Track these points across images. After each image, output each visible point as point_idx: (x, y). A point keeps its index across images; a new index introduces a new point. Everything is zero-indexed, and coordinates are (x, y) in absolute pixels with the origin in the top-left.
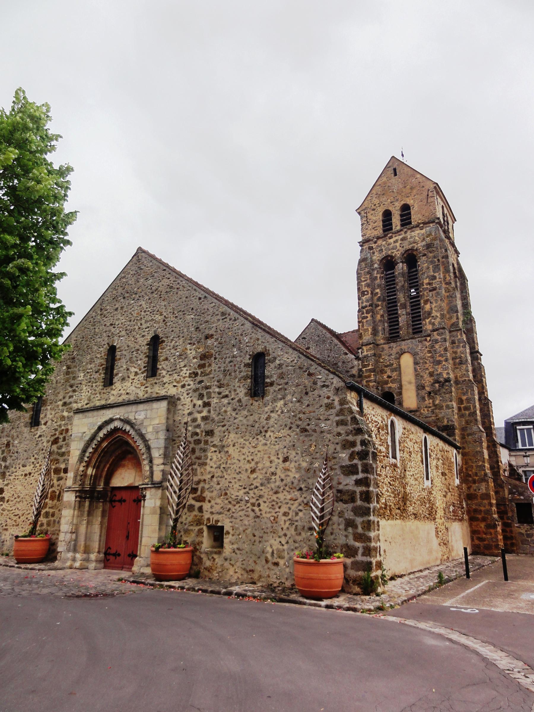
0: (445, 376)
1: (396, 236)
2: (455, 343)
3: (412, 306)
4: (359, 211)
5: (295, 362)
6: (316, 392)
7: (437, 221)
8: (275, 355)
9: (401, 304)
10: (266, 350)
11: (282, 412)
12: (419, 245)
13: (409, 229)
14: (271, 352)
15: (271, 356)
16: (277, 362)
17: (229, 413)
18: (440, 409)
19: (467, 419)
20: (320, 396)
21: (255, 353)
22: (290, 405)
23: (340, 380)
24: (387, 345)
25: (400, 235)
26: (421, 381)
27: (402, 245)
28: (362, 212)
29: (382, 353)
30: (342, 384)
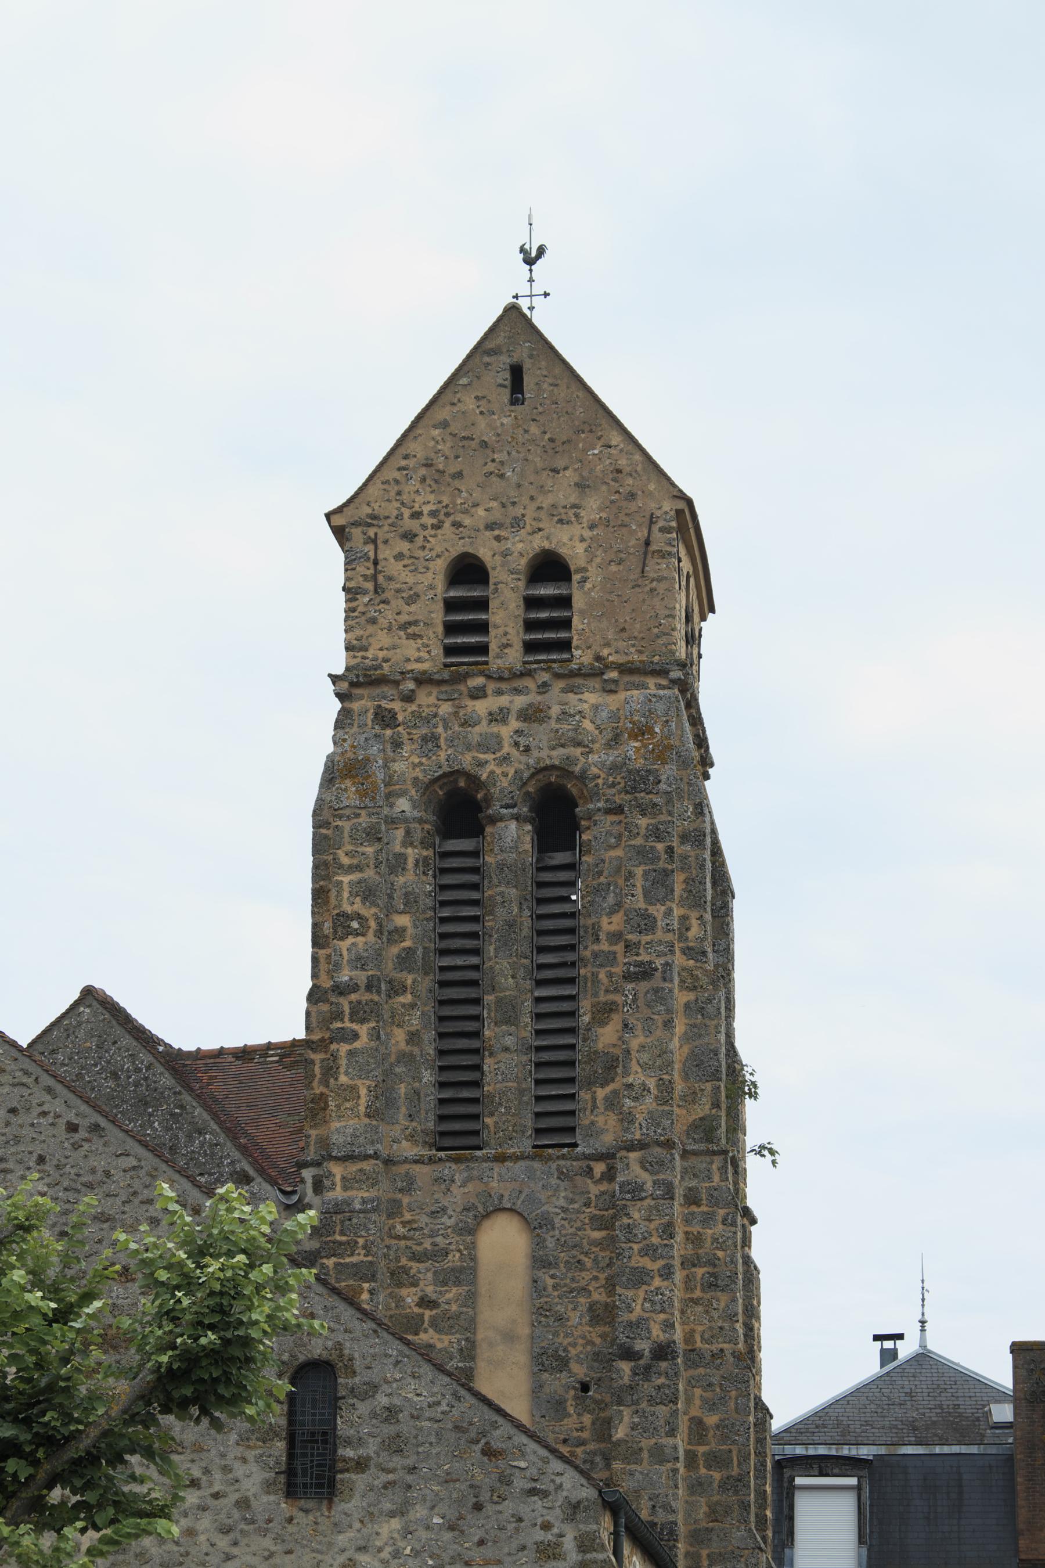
0: (657, 1333)
1: (499, 693)
2: (697, 1203)
3: (539, 1016)
4: (338, 521)
5: (444, 1407)
6: (508, 1507)
7: (676, 674)
8: (374, 1376)
9: (499, 1001)
10: (341, 1356)
11: (396, 1554)
12: (593, 758)
13: (558, 676)
14: (358, 1364)
15: (357, 1380)
16: (383, 1400)
17: (202, 1538)
18: (626, 1460)
19: (715, 1499)
20: (520, 1520)
21: (302, 1358)
22: (423, 1534)
23: (584, 1481)
24: (425, 1169)
25: (517, 691)
26: (556, 1334)
27: (523, 741)
28: (356, 533)
29: (406, 1200)
30: (588, 1493)
